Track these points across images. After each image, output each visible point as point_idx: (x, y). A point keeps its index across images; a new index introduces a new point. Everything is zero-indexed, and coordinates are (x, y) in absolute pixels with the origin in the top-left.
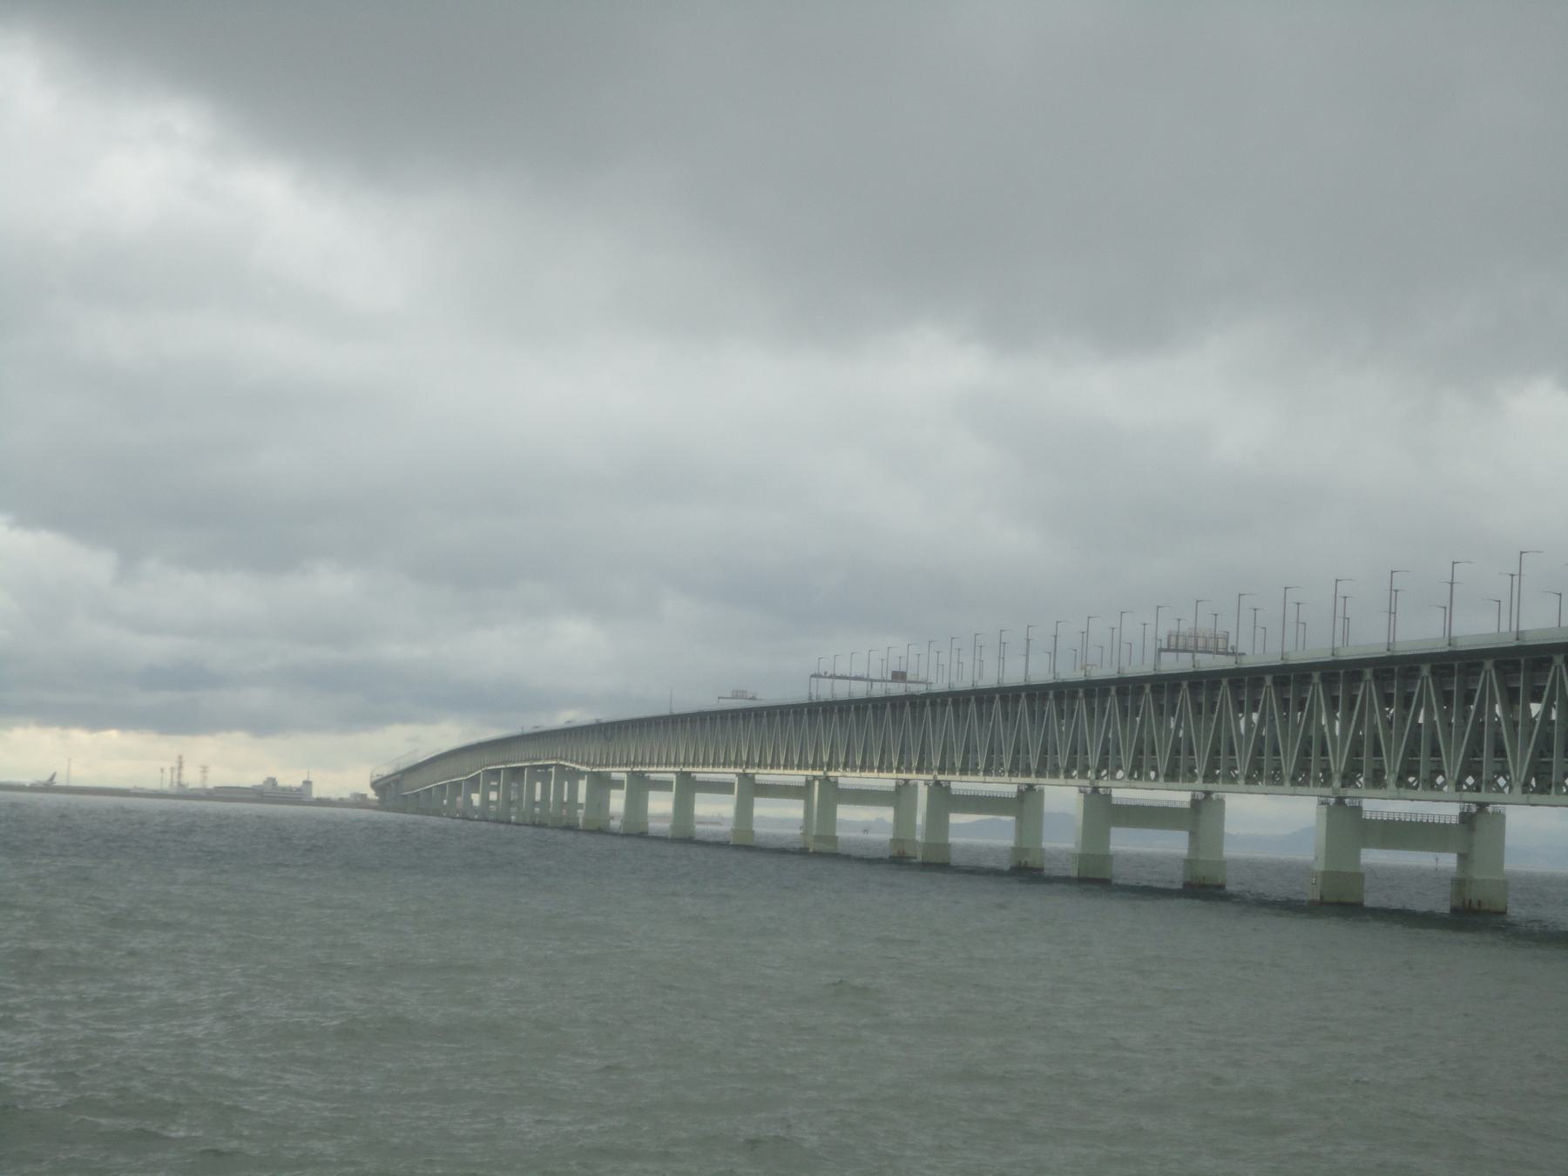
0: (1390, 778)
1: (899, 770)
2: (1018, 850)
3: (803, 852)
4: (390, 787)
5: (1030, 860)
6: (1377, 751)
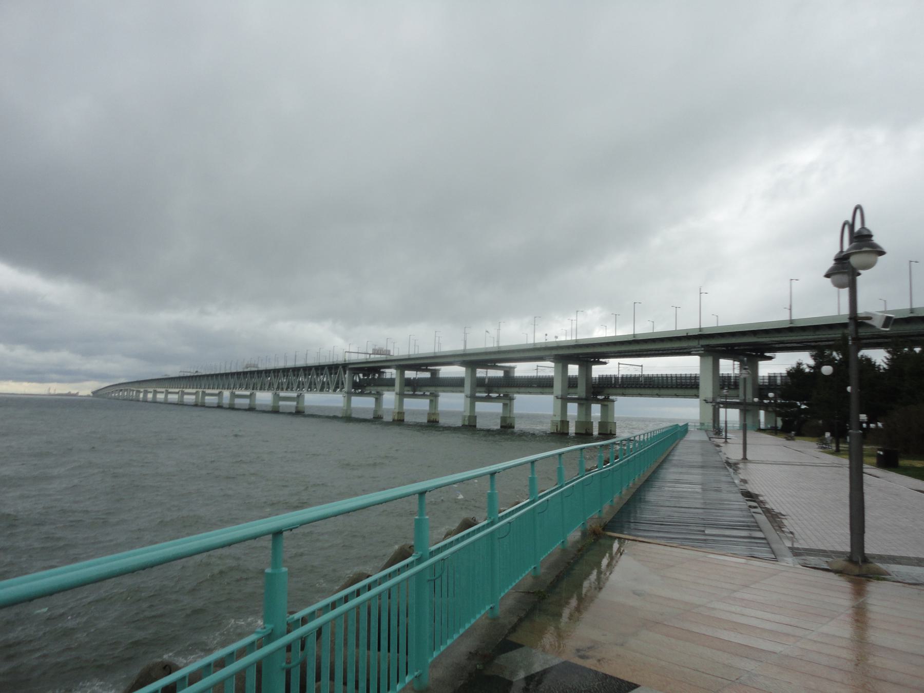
0: (258, 388)
1: (196, 388)
2: (218, 403)
3: (177, 404)
4: (95, 393)
5: (220, 405)
6: (292, 384)
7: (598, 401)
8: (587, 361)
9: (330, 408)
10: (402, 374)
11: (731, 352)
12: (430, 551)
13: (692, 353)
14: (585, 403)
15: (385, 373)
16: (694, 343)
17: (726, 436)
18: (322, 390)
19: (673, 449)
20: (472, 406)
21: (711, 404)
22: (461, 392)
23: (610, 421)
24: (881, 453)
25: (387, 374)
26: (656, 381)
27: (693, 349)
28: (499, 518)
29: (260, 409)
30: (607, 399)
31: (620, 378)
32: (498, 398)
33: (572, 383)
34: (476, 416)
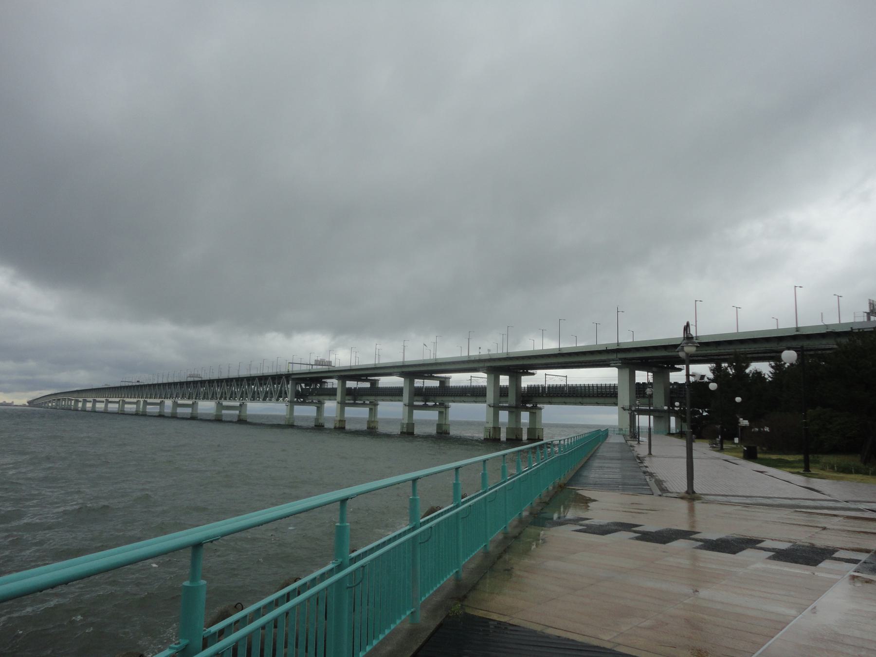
3: (117, 413)
5: (162, 414)
6: (226, 394)
7: (527, 409)
8: (517, 373)
9: (275, 417)
10: (344, 384)
11: (644, 364)
12: (350, 558)
13: (611, 365)
14: (515, 411)
15: (327, 383)
16: (613, 356)
17: (639, 439)
18: (264, 400)
19: (597, 449)
20: (411, 414)
21: (627, 412)
22: (399, 401)
23: (537, 427)
24: (745, 449)
25: (329, 383)
26: (579, 390)
27: (612, 362)
28: (421, 523)
29: (229, 419)
30: (535, 407)
31: (547, 388)
32: (435, 406)
33: (503, 392)
34: (414, 424)
